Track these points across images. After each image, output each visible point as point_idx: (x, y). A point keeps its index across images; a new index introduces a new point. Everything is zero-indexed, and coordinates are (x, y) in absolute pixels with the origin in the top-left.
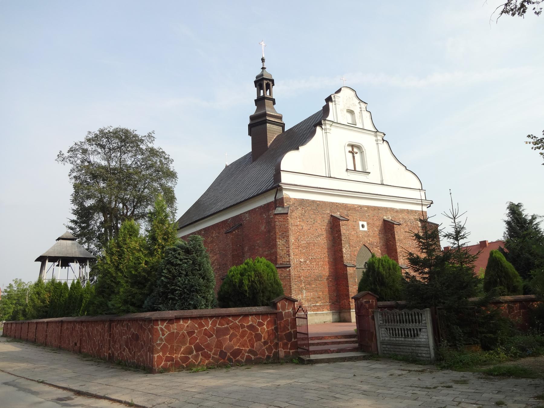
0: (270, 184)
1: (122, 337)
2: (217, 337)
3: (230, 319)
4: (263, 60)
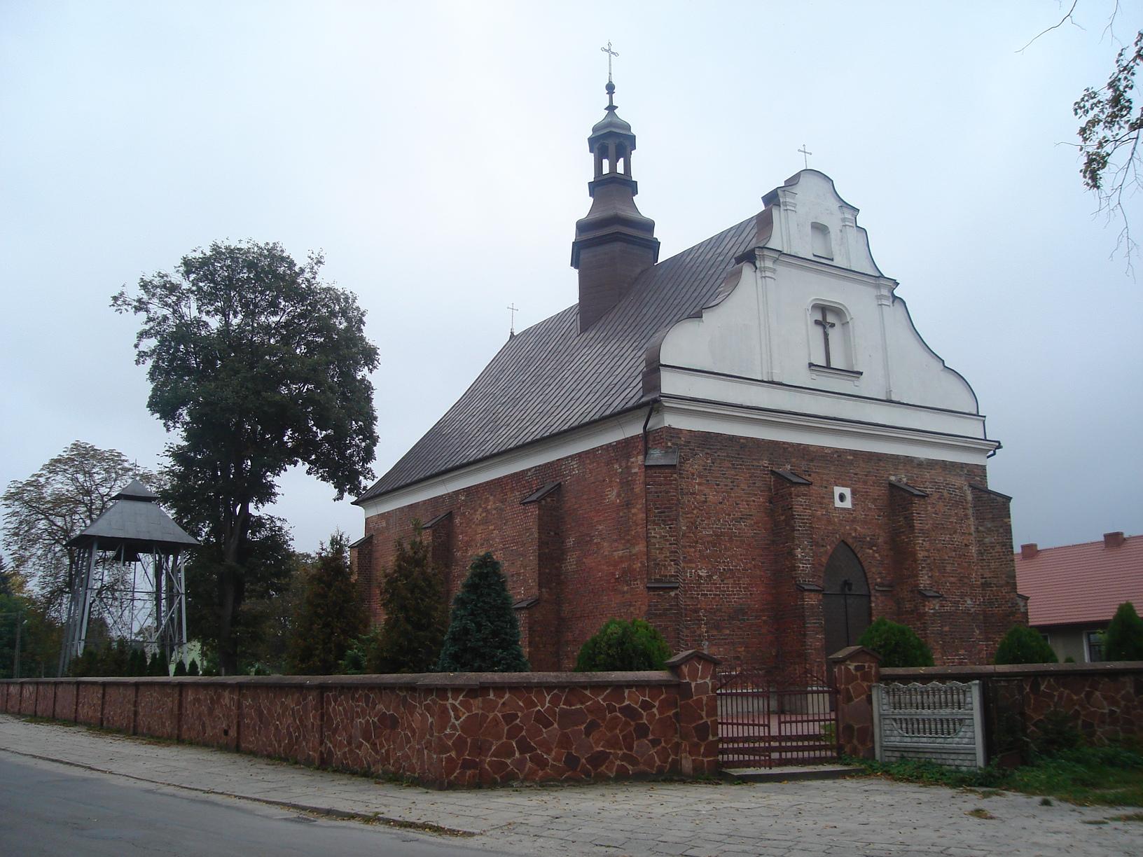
0: (633, 393)
1: (352, 720)
2: (561, 726)
3: (588, 693)
4: (610, 88)
